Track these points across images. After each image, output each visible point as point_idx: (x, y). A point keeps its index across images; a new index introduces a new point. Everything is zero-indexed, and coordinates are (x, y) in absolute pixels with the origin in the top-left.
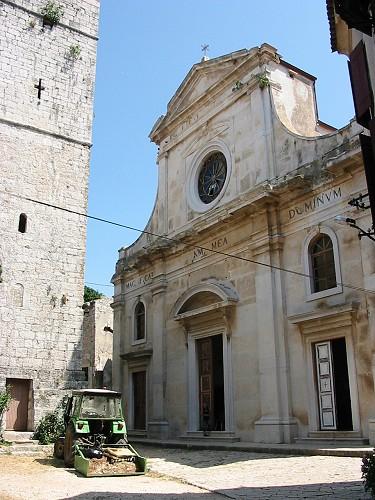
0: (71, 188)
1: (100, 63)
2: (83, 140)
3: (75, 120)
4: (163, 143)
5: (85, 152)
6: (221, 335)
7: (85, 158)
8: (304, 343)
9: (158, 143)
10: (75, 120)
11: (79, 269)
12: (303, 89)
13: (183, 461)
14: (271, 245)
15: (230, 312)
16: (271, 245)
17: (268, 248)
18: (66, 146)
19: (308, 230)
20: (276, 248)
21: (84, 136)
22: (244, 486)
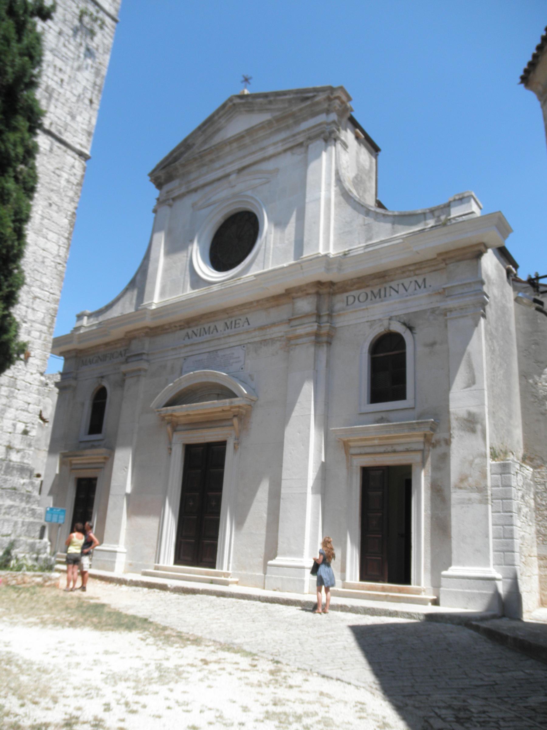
0: (54, 207)
1: (117, 52)
2: (78, 147)
3: (73, 117)
4: (166, 188)
5: (78, 164)
6: (223, 444)
7: (79, 171)
8: (349, 467)
9: (159, 186)
10: (73, 117)
11: (47, 321)
12: (365, 156)
13: (317, 479)
14: (317, 335)
15: (242, 417)
16: (317, 335)
17: (313, 338)
18: (55, 148)
19: (372, 323)
20: (324, 339)
21: (80, 141)
22: (286, 606)
